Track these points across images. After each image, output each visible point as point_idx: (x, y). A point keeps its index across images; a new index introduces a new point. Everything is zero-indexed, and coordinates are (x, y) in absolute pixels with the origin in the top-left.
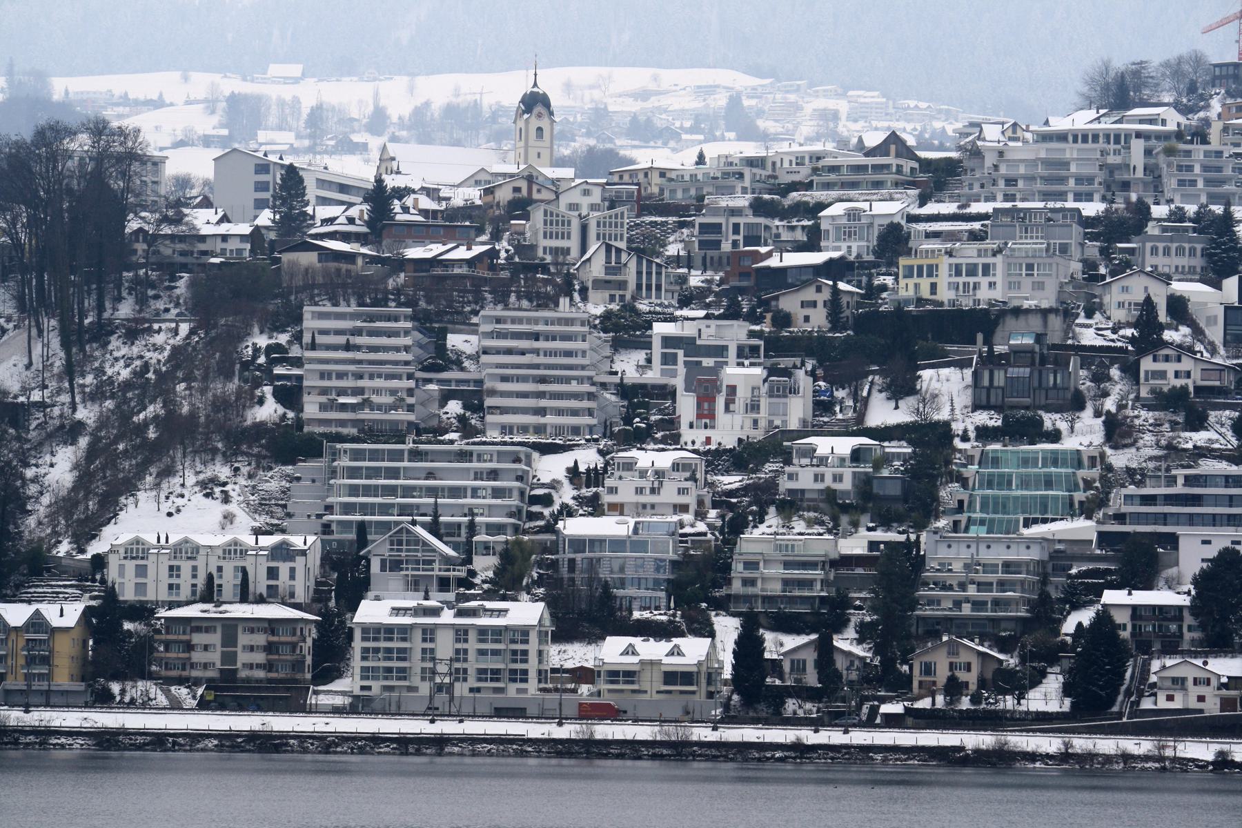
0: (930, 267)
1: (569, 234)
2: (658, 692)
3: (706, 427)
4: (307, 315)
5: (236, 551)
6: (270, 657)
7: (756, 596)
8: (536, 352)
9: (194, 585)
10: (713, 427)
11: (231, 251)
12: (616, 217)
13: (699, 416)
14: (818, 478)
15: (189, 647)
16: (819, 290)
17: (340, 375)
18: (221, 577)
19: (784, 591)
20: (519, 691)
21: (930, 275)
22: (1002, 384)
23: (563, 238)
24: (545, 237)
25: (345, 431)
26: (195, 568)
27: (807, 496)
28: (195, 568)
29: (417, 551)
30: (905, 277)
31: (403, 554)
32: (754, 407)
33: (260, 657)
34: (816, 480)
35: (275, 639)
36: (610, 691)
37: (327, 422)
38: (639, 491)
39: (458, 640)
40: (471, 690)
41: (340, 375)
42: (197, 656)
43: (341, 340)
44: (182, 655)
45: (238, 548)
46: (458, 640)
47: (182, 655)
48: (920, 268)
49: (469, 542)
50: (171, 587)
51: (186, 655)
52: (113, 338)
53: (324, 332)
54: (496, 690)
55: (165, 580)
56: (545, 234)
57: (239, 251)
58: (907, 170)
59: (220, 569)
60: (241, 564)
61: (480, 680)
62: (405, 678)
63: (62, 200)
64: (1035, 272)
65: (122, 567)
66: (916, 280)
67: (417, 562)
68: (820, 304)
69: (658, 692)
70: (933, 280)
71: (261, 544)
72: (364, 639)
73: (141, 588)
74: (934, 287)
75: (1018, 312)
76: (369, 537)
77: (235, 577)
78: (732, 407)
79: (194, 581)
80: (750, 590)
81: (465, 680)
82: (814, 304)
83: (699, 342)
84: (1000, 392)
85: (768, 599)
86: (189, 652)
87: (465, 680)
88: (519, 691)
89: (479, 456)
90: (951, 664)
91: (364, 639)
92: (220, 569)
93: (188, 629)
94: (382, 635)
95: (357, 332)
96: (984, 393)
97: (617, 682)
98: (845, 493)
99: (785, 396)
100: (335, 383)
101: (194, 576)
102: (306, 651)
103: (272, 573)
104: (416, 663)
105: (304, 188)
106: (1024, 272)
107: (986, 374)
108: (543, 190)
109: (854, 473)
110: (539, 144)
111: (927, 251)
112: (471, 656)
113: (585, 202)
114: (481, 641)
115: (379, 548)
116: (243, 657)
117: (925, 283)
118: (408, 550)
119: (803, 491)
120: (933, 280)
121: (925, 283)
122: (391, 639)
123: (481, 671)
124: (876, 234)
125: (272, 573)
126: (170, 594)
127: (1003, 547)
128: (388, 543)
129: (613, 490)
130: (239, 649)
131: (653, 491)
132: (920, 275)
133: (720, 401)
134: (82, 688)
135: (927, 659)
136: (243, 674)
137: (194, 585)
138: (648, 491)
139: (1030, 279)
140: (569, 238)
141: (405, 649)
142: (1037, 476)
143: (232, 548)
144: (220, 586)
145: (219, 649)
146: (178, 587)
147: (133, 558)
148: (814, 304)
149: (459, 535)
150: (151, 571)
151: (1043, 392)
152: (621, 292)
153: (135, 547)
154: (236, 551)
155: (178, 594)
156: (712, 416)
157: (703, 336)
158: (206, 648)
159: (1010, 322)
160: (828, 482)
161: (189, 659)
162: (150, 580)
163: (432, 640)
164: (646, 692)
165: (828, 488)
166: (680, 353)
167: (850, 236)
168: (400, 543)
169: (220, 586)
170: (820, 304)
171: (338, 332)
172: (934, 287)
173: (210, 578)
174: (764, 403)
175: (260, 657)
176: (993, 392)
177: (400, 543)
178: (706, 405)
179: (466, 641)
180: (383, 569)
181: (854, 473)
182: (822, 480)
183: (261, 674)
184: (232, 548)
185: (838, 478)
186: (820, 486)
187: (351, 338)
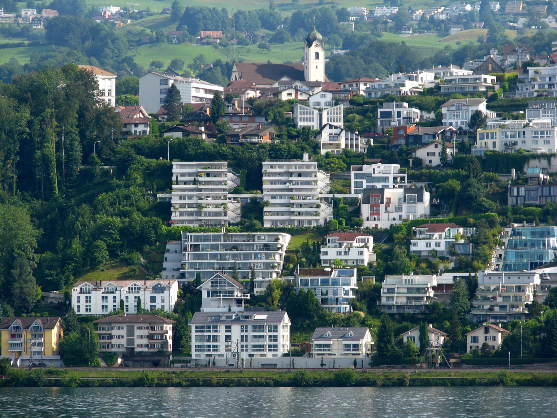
0: (492, 134)
1: (313, 119)
2: (341, 354)
3: (375, 220)
4: (174, 167)
5: (135, 288)
6: (151, 341)
7: (393, 305)
8: (290, 182)
9: (115, 306)
10: (379, 219)
11: (140, 132)
12: (337, 110)
13: (372, 214)
14: (428, 245)
15: (110, 337)
16: (436, 146)
17: (191, 197)
18: (127, 301)
19: (407, 303)
20: (273, 355)
21: (492, 138)
22: (523, 194)
23: (310, 121)
24: (300, 121)
25: (192, 226)
26: (115, 297)
27: (423, 254)
28: (115, 297)
29: (225, 286)
30: (480, 139)
31: (218, 288)
32: (400, 209)
33: (145, 341)
34: (427, 246)
35: (153, 332)
36: (318, 355)
37: (183, 221)
38: (339, 253)
39: (242, 331)
40: (250, 355)
41: (191, 197)
42: (114, 341)
43: (192, 178)
44: (107, 341)
45: (136, 287)
46: (242, 331)
47: (107, 341)
48: (487, 134)
49: (252, 282)
50: (103, 307)
51: (109, 341)
52: (376, 17)
53: (183, 175)
54: (262, 355)
55: (100, 303)
56: (300, 119)
57: (144, 132)
58: (489, 81)
59: (127, 298)
60: (137, 295)
61: (253, 350)
62: (217, 350)
63: (88, 81)
64: (545, 135)
65: (79, 298)
66: (485, 140)
67: (225, 292)
68: (437, 154)
69: (341, 354)
70: (494, 140)
71: (147, 285)
72: (196, 331)
73: (88, 309)
74: (494, 143)
75: (535, 157)
76: (202, 280)
77: (135, 301)
78: (388, 209)
79: (115, 304)
80: (390, 303)
81: (246, 350)
82: (434, 154)
83: (373, 175)
84: (523, 198)
85: (398, 307)
86: (111, 339)
87: (246, 350)
88: (273, 355)
89: (258, 237)
90: (486, 337)
91: (196, 331)
92: (127, 298)
93: (110, 328)
94: (205, 329)
95: (198, 174)
96: (515, 198)
97: (320, 350)
98: (441, 252)
99: (415, 203)
100: (187, 201)
101: (115, 302)
102: (168, 338)
103: (153, 299)
104: (222, 343)
105: (180, 96)
106: (539, 135)
107: (515, 189)
108: (303, 94)
109: (446, 242)
110: (317, 61)
111: (491, 126)
112: (249, 338)
113: (323, 101)
114: (254, 331)
115: (206, 286)
116: (137, 341)
117: (490, 142)
118: (221, 286)
119: (421, 252)
120: (494, 140)
121: (490, 142)
122: (210, 331)
123: (255, 346)
124: (470, 116)
125: (153, 299)
126: (103, 311)
127: (517, 277)
128: (210, 283)
129: (326, 253)
130: (135, 337)
131: (346, 253)
132: (487, 138)
133: (383, 206)
134: (59, 358)
135: (473, 334)
136: (137, 350)
137: (115, 306)
138: (343, 253)
139: (542, 139)
140: (313, 121)
141: (217, 336)
142: (105, 334)
143: (133, 287)
144: (127, 306)
145: (125, 337)
146: (107, 307)
147: (84, 293)
148: (434, 154)
149: (248, 278)
150: (93, 300)
151: (544, 198)
152: (337, 150)
153: (85, 287)
154: (135, 288)
155: (107, 311)
156: (378, 214)
157: (376, 172)
158: (119, 337)
159: (533, 163)
160: (433, 247)
161: (111, 343)
162: (92, 304)
163: (230, 331)
164: (335, 355)
165: (433, 250)
166: (364, 181)
167: (457, 117)
168: (216, 282)
169: (127, 306)
170: (437, 154)
171: (190, 174)
172: (494, 143)
173: (122, 302)
174: (405, 206)
175: (145, 341)
176: (519, 198)
177: (216, 282)
178: (375, 209)
179: (246, 331)
180: (208, 296)
181: (446, 242)
182: (430, 246)
183: (145, 350)
184: (133, 287)
185: (438, 245)
186: (429, 249)
187: (196, 178)
